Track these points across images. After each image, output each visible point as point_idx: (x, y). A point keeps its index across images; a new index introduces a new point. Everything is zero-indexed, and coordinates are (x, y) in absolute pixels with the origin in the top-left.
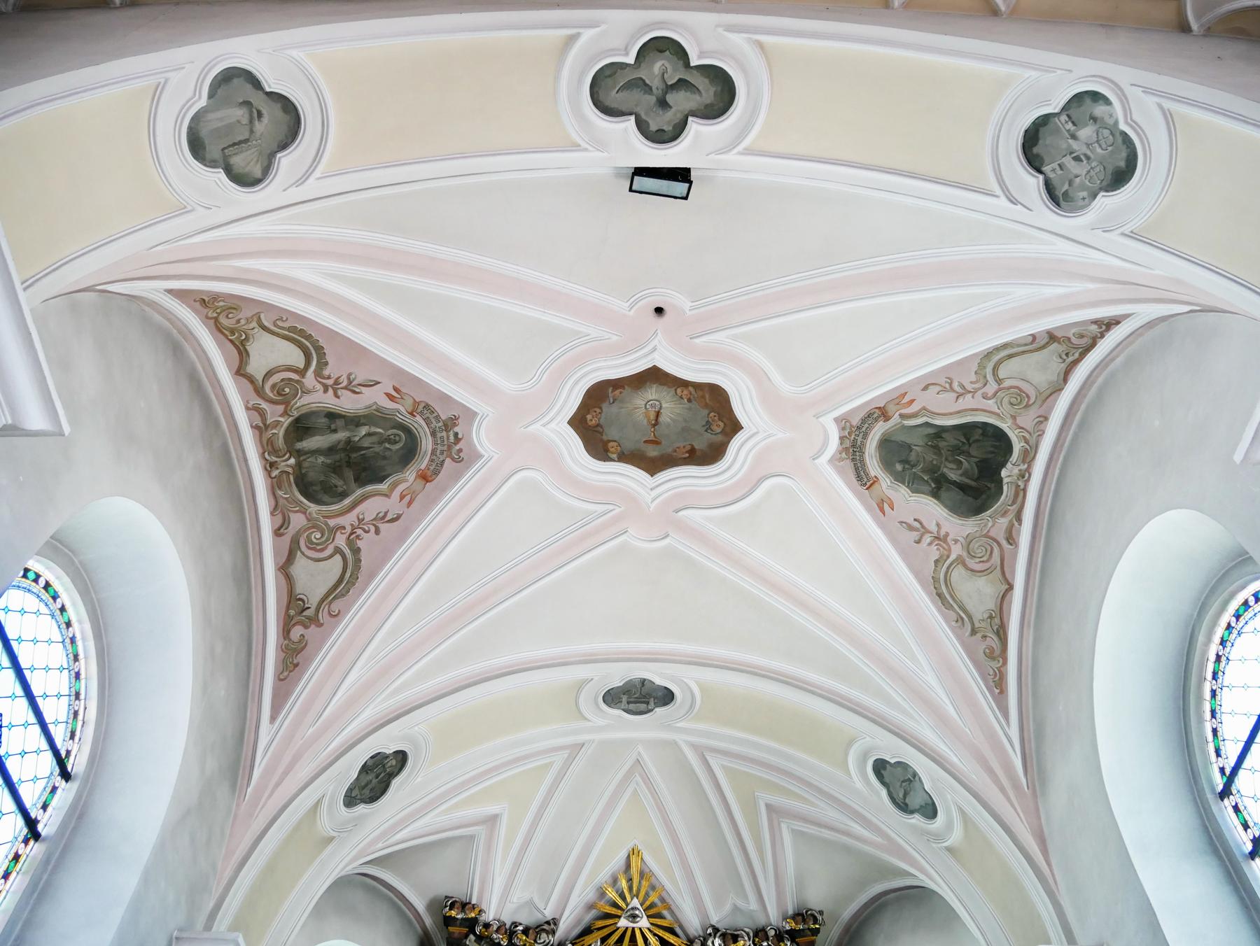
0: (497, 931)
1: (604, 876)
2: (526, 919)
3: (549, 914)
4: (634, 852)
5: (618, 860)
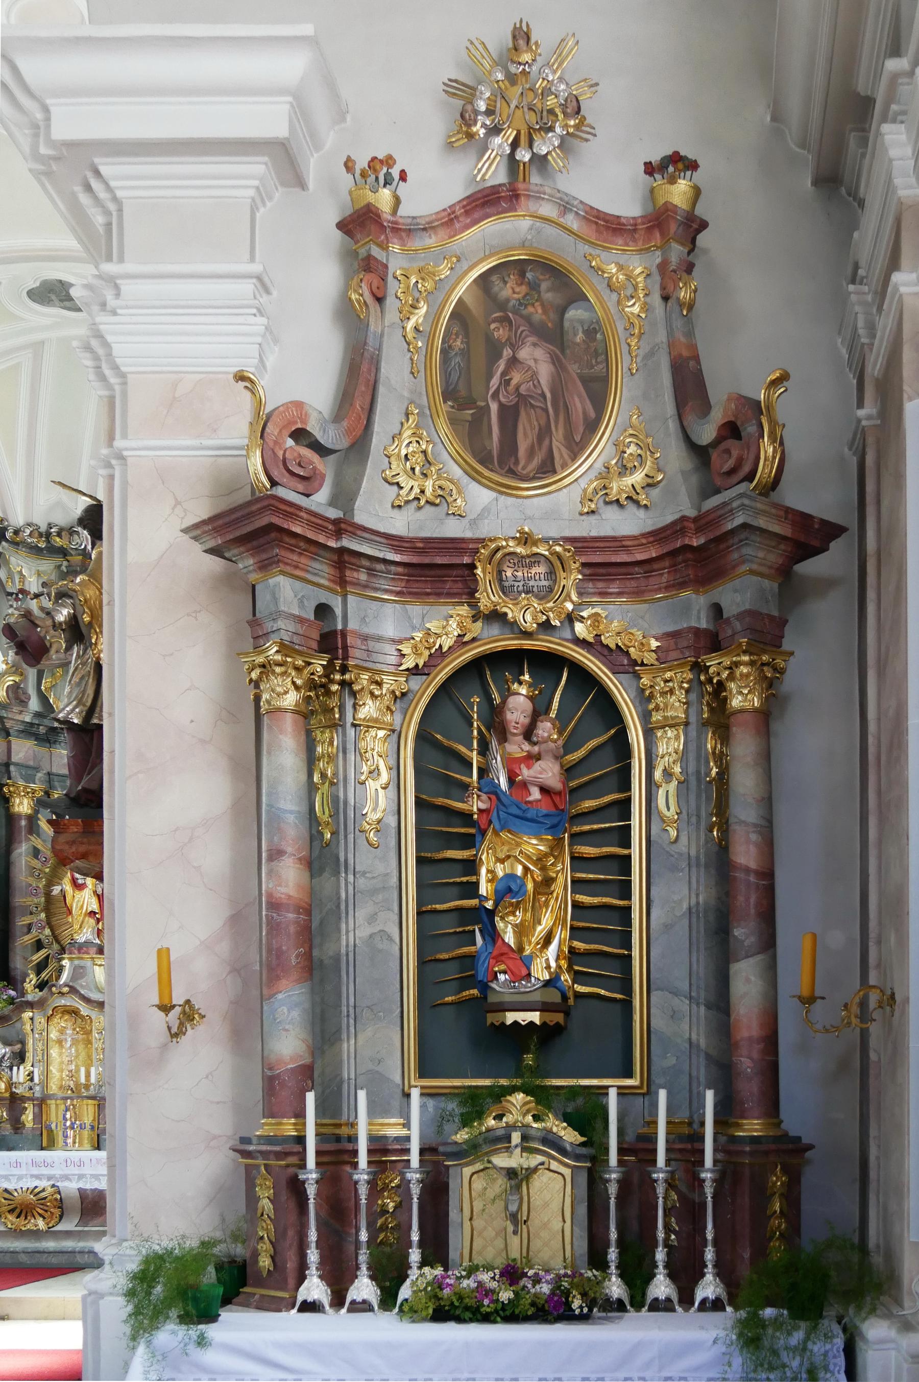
0: (30, 535)
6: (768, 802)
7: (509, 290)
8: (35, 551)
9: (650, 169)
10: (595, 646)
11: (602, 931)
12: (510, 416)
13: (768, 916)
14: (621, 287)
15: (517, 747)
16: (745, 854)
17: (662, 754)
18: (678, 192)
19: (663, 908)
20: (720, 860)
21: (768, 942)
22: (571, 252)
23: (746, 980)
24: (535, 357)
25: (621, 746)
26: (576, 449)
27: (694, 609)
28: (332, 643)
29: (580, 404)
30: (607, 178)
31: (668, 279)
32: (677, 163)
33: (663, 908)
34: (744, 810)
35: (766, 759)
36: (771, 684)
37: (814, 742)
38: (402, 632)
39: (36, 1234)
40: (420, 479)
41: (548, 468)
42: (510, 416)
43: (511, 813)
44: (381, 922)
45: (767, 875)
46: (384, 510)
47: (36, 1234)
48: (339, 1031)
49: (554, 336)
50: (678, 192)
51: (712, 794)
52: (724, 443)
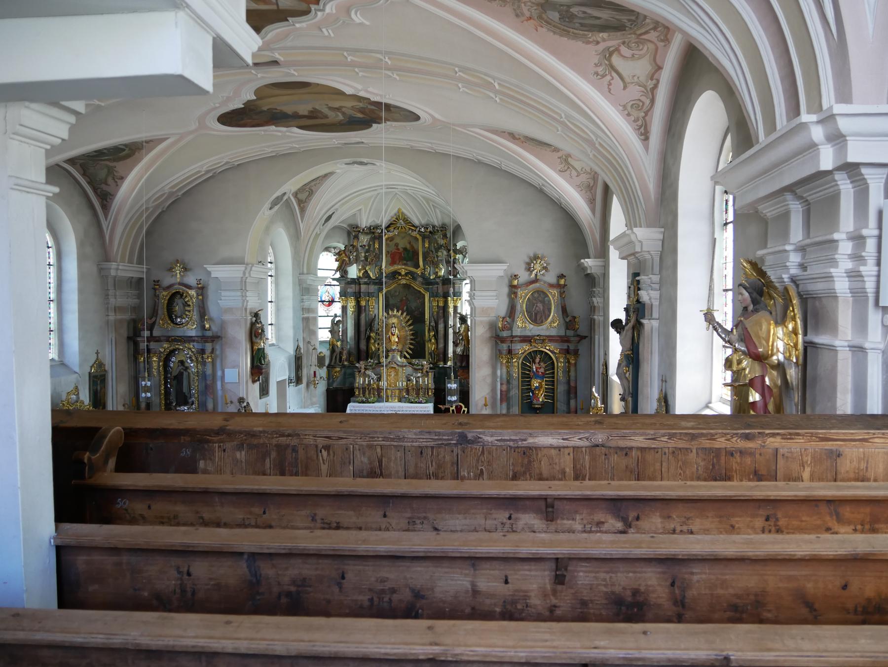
1: (393, 213)
2: (373, 224)
3: (379, 222)
4: (399, 209)
5: (395, 211)
6: (576, 377)
7: (536, 295)
8: (367, 234)
9: (574, 318)
10: (549, 350)
11: (551, 393)
12: (536, 315)
13: (576, 393)
14: (553, 295)
15: (537, 365)
16: (572, 384)
17: (560, 364)
18: (562, 282)
19: (561, 389)
20: (569, 382)
21: (576, 397)
22: (545, 289)
23: (572, 402)
24: (540, 305)
25: (553, 363)
26: (546, 319)
27: (565, 346)
28: (510, 352)
29: (547, 312)
30: (551, 278)
31: (561, 294)
32: (562, 276)
33: (561, 389)
34: (572, 378)
35: (576, 370)
36: (576, 360)
37: (582, 363)
38: (522, 349)
39: (268, 147)
40: (522, 326)
41: (542, 322)
42: (536, 315)
43: (536, 376)
44: (515, 392)
45: (576, 387)
46: (517, 332)
47: (268, 147)
48: (516, 427)
49: (543, 302)
50: (562, 282)
51: (567, 372)
52: (569, 322)
